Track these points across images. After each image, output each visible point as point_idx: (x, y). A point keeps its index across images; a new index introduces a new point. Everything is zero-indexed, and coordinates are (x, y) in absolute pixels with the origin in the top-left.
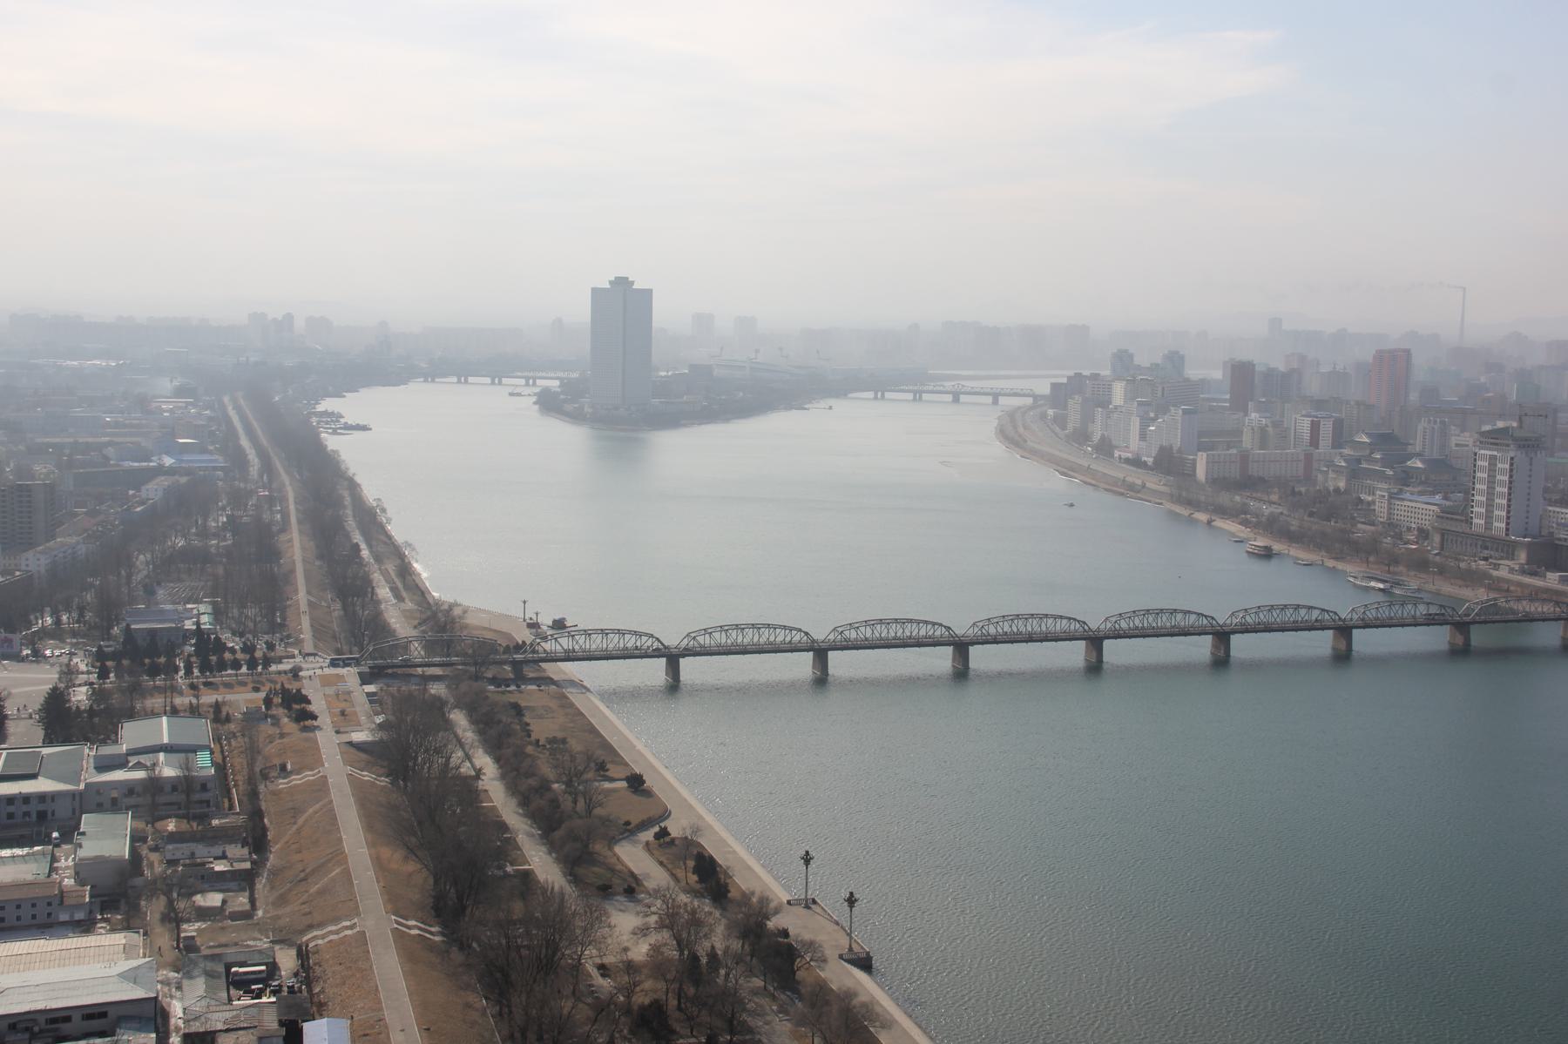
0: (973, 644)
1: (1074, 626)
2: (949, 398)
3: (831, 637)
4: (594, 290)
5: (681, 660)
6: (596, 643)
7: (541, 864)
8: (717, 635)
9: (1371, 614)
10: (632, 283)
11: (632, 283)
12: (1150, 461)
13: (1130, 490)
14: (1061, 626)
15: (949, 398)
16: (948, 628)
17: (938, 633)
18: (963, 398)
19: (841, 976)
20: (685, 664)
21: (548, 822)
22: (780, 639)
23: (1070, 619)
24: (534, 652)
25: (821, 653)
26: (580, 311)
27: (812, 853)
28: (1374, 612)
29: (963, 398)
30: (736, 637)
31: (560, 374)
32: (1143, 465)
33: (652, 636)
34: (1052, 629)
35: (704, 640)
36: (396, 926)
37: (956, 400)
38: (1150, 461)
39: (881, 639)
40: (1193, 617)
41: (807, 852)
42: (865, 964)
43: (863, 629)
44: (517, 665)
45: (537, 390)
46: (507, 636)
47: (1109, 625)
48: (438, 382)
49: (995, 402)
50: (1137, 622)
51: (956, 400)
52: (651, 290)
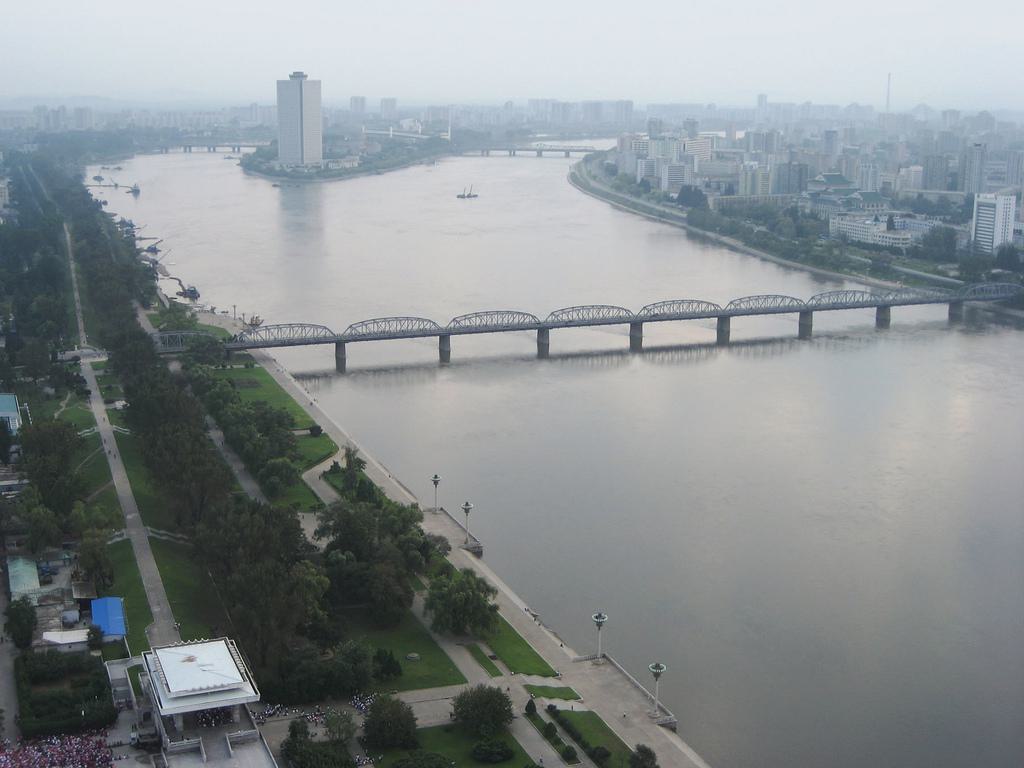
0: (348, 341)
1: (623, 314)
2: (535, 153)
3: (452, 325)
4: (279, 82)
5: (892, 308)
6: (286, 334)
7: (249, 487)
8: (371, 326)
9: (825, 301)
10: (306, 76)
11: (306, 76)
12: (675, 196)
13: (662, 217)
14: (613, 313)
15: (535, 153)
16: (533, 317)
17: (527, 320)
18: (544, 153)
19: (460, 559)
20: (455, 341)
21: (253, 466)
22: (516, 321)
23: (619, 308)
24: (242, 341)
25: (444, 337)
26: (269, 96)
27: (440, 477)
28: (827, 299)
29: (544, 153)
30: (487, 321)
31: (256, 144)
32: (671, 200)
33: (325, 328)
34: (607, 315)
35: (362, 330)
36: (151, 534)
37: (540, 154)
38: (675, 196)
39: (841, 303)
40: (704, 305)
41: (436, 477)
42: (478, 553)
43: (308, 329)
44: (229, 351)
45: (241, 156)
46: (223, 331)
47: (814, 302)
48: (493, 156)
49: (567, 156)
50: (575, 316)
51: (540, 154)
52: (320, 82)
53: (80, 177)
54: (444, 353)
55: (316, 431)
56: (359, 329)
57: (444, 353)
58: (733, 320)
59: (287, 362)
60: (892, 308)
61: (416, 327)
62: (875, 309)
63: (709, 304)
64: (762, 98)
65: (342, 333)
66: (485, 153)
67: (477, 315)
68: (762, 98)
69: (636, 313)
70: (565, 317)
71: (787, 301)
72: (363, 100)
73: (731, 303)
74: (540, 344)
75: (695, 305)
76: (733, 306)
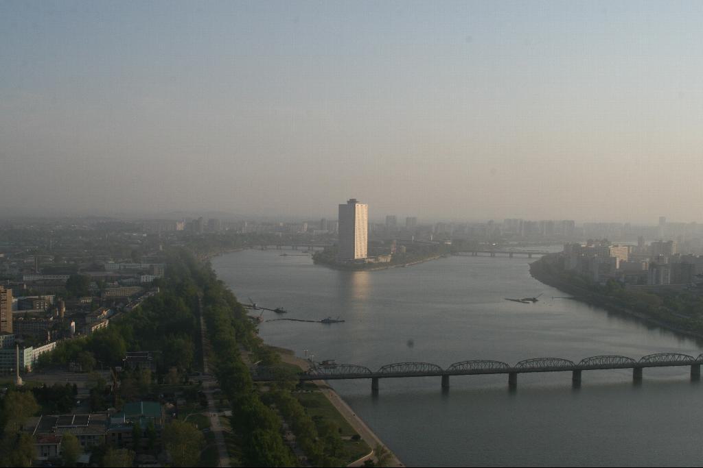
1: (568, 364)
4: (340, 205)
5: (643, 369)
14: (560, 364)
16: (507, 365)
17: (435, 369)
34: (542, 365)
39: (482, 369)
47: (644, 361)
53: (209, 264)
54: (375, 388)
55: (356, 437)
56: (388, 369)
57: (375, 388)
58: (645, 370)
59: (336, 394)
60: (643, 369)
61: (426, 370)
62: (690, 366)
63: (627, 358)
64: (662, 219)
65: (376, 371)
66: (474, 254)
67: (468, 362)
68: (662, 219)
69: (577, 363)
70: (591, 363)
71: (629, 361)
72: (573, 222)
73: (519, 363)
74: (635, 377)
75: (618, 359)
76: (644, 361)
